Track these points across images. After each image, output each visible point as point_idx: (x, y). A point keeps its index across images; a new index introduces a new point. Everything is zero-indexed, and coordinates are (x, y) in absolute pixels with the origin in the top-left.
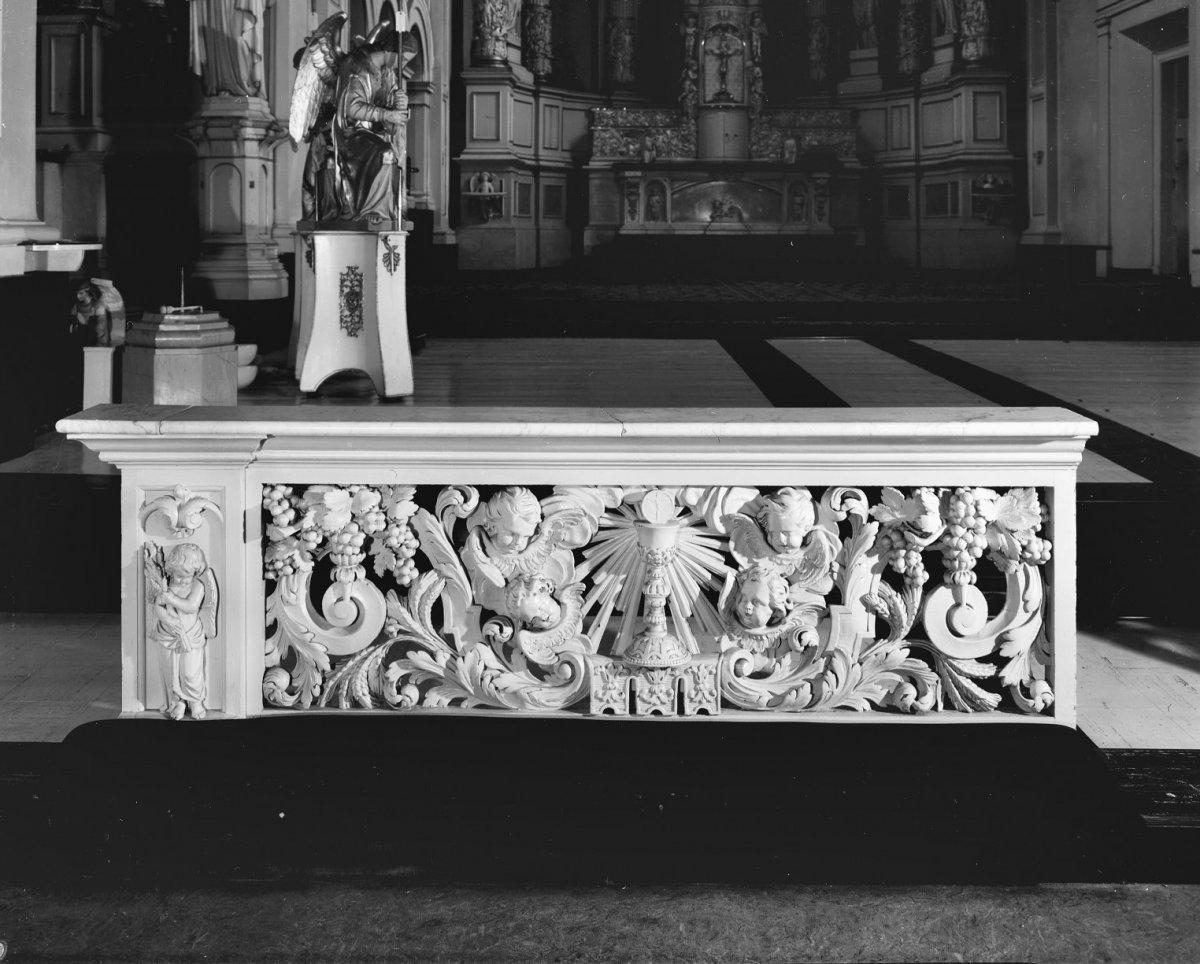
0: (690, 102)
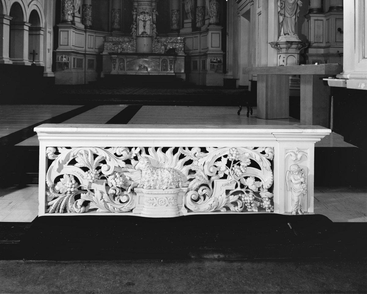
0: (134, 35)
